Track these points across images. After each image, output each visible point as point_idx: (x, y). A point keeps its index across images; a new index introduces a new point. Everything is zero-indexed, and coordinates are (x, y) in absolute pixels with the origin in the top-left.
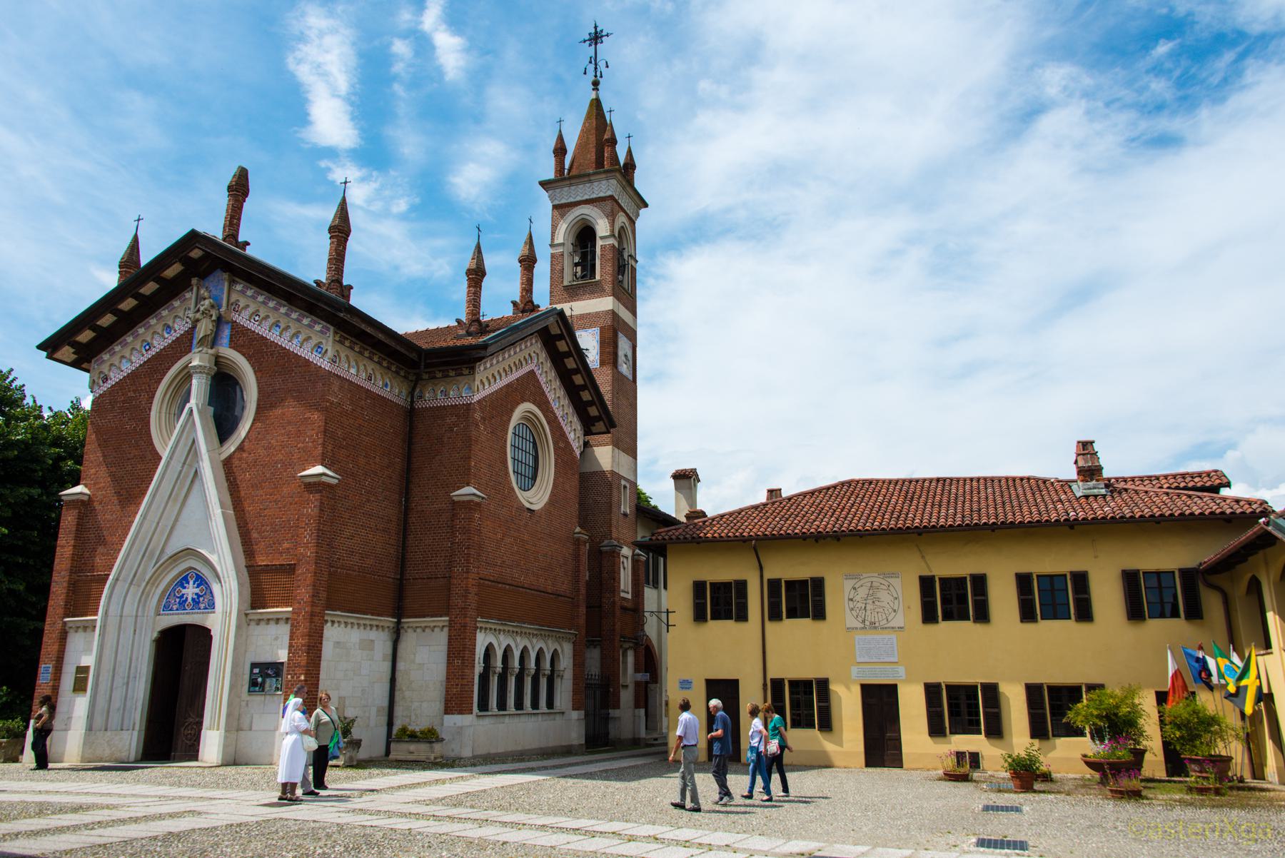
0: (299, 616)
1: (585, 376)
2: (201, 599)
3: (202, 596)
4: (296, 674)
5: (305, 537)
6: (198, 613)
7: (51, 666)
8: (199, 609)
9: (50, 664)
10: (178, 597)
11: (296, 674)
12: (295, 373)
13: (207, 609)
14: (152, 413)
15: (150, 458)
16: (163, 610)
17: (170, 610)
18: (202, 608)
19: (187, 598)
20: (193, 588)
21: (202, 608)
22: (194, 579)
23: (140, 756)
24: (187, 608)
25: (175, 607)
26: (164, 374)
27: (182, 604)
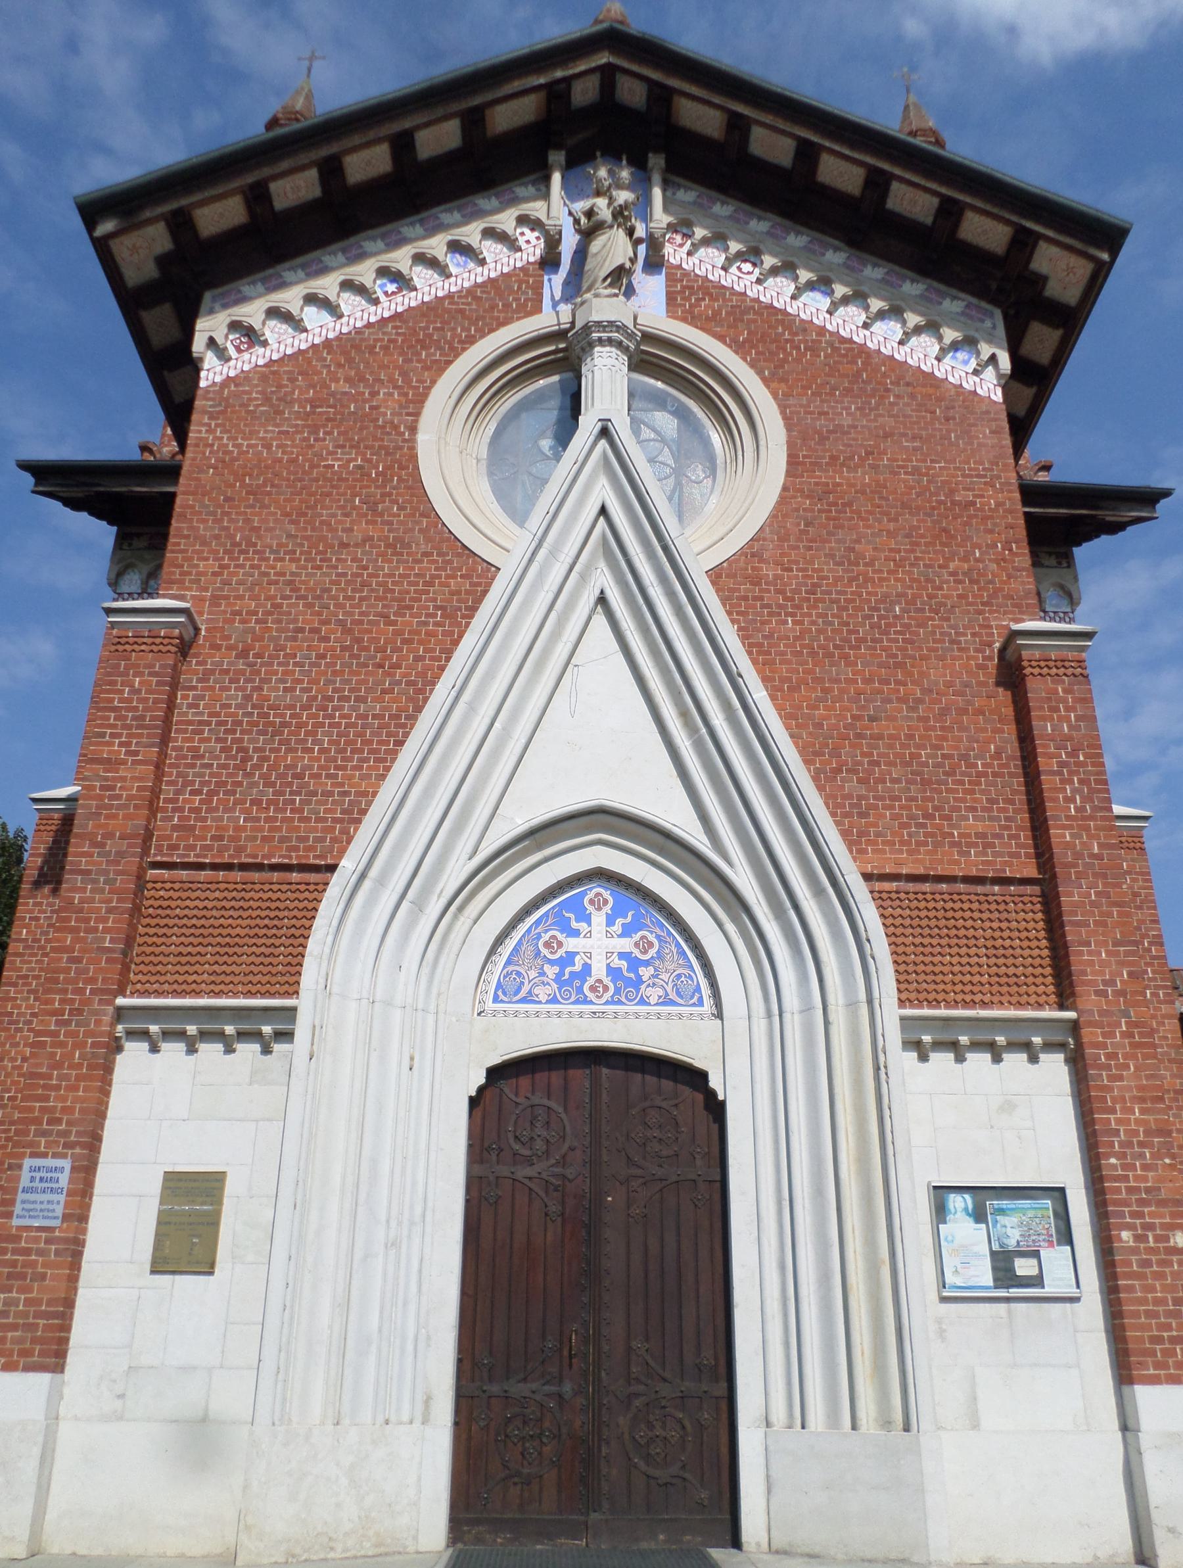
0: (1112, 1035)
1: (357, 139)
2: (646, 973)
3: (647, 963)
4: (1150, 1227)
5: (1072, 800)
6: (637, 1016)
7: (66, 1164)
8: (642, 1002)
9: (64, 1156)
10: (552, 963)
11: (1150, 1227)
12: (897, 397)
13: (672, 1003)
14: (421, 437)
15: (423, 548)
16: (496, 999)
17: (523, 1000)
18: (653, 1000)
19: (576, 933)
20: (609, 954)
21: (653, 1000)
22: (607, 909)
23: (488, 112)
24: (591, 996)
25: (542, 993)
26: (455, 353)
27: (569, 982)
